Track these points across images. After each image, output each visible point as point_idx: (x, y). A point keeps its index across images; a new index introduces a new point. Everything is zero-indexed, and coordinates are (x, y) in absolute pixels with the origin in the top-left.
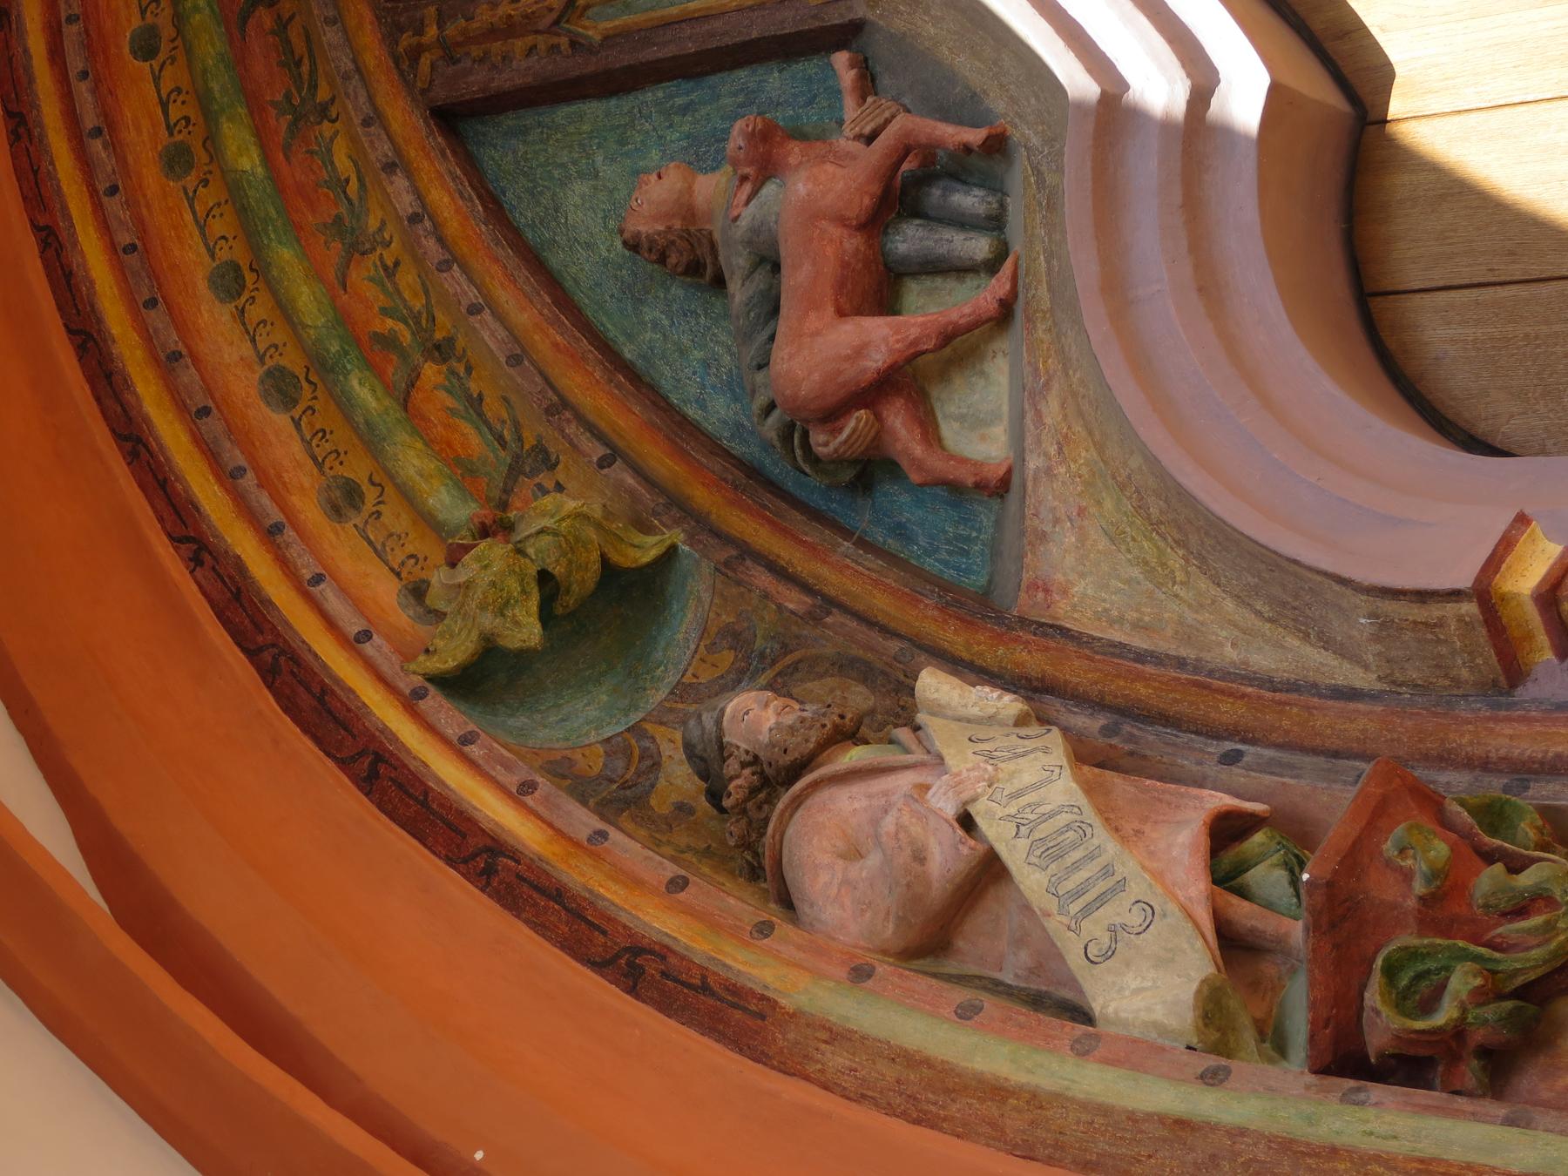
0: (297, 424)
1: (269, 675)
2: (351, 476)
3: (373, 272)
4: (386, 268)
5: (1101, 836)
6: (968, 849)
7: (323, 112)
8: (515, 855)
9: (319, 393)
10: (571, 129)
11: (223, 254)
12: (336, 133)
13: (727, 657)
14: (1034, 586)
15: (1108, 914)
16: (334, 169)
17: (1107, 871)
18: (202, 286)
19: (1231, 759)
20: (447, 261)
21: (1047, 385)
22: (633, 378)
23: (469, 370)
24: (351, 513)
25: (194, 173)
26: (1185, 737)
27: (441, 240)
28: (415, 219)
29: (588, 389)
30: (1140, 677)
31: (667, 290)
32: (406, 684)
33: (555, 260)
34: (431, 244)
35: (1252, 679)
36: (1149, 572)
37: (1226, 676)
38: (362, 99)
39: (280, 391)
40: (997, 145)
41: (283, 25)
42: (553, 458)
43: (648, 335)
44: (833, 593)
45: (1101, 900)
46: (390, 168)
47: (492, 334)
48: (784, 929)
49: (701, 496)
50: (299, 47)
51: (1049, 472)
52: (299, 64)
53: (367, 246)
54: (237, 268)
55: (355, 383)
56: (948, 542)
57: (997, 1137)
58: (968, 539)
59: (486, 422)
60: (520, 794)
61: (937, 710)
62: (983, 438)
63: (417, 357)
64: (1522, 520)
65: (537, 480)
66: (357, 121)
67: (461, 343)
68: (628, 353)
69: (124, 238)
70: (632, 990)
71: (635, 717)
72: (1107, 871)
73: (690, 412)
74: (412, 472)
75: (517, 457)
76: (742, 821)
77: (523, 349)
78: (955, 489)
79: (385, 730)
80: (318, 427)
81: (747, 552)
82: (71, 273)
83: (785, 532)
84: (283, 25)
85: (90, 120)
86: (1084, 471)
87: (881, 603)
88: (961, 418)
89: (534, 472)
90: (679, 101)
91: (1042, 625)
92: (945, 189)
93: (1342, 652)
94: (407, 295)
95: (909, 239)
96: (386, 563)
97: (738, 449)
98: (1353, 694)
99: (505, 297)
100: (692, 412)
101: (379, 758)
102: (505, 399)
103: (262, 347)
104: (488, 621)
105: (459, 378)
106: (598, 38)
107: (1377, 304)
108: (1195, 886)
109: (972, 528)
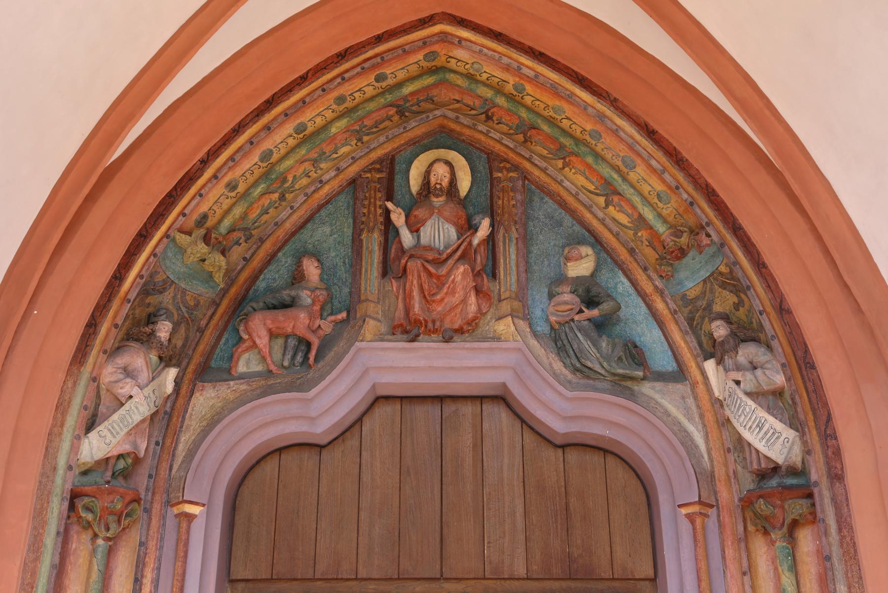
0: (255, 164)
1: (169, 195)
5: (126, 430)
6: (123, 400)
7: (360, 140)
8: (120, 286)
11: (309, 124)
13: (192, 303)
14: (203, 386)
15: (109, 435)
17: (118, 433)
18: (299, 121)
19: (157, 443)
22: (271, 258)
23: (276, 208)
26: (163, 431)
27: (314, 191)
28: (321, 182)
29: (268, 246)
30: (178, 418)
32: (172, 233)
33: (309, 225)
34: (313, 188)
35: (176, 445)
36: (203, 417)
37: (177, 439)
40: (310, 367)
41: (389, 118)
45: (112, 433)
46: (338, 169)
48: (105, 356)
49: (233, 290)
50: (381, 126)
52: (376, 127)
54: (305, 130)
57: (53, 426)
60: (140, 276)
61: (168, 373)
63: (280, 191)
64: (204, 505)
67: (284, 204)
68: (280, 254)
69: (307, 100)
70: (87, 325)
71: (177, 281)
72: (118, 433)
75: (249, 229)
76: (138, 332)
78: (231, 357)
79: (153, 236)
81: (218, 305)
83: (222, 316)
84: (389, 118)
85: (346, 76)
87: (201, 347)
89: (245, 235)
93: (178, 470)
98: (171, 470)
100: (262, 277)
101: (145, 237)
104: (189, 250)
107: (278, 453)
108: (115, 453)
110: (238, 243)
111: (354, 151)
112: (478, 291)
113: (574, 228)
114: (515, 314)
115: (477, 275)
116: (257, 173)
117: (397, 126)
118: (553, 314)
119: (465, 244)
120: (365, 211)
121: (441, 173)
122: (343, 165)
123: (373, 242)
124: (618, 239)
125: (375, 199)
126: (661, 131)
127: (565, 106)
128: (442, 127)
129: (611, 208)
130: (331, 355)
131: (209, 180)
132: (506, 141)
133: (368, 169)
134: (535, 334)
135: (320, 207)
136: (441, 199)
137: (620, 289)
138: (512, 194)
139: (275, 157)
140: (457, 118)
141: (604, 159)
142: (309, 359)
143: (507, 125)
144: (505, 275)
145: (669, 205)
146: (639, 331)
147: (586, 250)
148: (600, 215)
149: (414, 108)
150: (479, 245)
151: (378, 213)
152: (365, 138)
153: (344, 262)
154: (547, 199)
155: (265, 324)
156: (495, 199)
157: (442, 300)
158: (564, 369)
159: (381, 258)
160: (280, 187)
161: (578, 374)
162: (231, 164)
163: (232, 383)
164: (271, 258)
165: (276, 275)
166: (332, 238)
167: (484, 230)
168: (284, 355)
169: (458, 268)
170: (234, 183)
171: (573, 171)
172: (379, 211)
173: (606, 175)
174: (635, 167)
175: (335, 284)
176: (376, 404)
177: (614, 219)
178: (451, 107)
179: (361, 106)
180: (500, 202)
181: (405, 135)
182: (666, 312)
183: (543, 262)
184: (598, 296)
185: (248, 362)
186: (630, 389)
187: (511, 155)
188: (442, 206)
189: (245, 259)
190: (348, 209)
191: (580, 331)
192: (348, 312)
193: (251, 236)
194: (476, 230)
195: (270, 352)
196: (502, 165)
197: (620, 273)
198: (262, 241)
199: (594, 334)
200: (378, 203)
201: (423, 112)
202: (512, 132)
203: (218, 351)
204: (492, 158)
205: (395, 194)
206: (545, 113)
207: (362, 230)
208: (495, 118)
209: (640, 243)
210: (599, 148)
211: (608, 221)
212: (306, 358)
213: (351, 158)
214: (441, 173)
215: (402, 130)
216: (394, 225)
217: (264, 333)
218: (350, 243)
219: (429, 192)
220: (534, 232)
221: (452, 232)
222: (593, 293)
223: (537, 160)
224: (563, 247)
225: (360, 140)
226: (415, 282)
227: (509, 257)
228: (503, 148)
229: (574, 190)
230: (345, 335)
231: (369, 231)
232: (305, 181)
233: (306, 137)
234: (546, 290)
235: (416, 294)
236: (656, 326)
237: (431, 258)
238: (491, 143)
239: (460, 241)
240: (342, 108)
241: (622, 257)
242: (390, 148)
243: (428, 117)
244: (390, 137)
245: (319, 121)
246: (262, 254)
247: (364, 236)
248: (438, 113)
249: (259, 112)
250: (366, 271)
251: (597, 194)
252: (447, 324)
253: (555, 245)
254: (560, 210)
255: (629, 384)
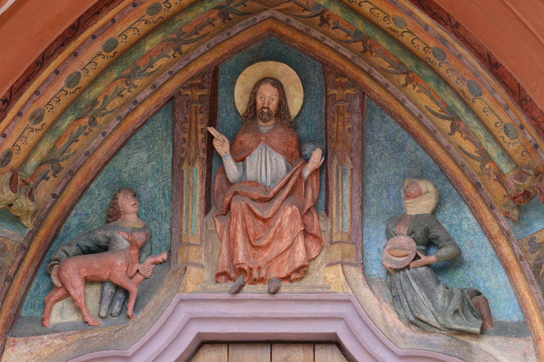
0: (62, 90)
2: (45, 117)
3: (119, 88)
4: (120, 92)
7: (178, 49)
9: (72, 94)
10: (165, 149)
11: (120, 40)
12: (169, 58)
14: (14, 341)
16: (156, 60)
18: (108, 38)
20: (121, 118)
21: (65, 339)
22: (84, 190)
24: (33, 122)
25: (150, 17)
27: (128, 114)
28: (135, 102)
29: (78, 179)
31: (110, 198)
33: (124, 151)
34: (127, 110)
38: (179, 67)
39: (72, 79)
42: (57, 175)
43: (97, 193)
44: (14, 282)
47: (96, 143)
49: (42, 232)
50: (202, 32)
51: (43, 342)
52: (196, 33)
53: (129, 82)
54: (115, 47)
55: (71, 118)
56: (34, 302)
58: (35, 308)
59: (69, 145)
62: (57, 315)
65: (50, 170)
66: (170, 70)
67: (95, 129)
68: (93, 186)
69: (117, 18)
73: (73, 212)
74: (42, 149)
77: (91, 155)
80: (61, 98)
82: (99, 13)
84: (211, 23)
86: (42, 353)
88: (63, 308)
89: (53, 167)
90: (166, 192)
91: (4, 346)
92: (122, 298)
94: (112, 102)
95: (109, 290)
96: (17, 140)
97: (62, 230)
99: (107, 145)
100: (73, 212)
102: (76, 151)
103: (87, 67)
105: (83, 131)
106: (183, 168)
109: (37, 309)
110: (45, 177)
111: (171, 64)
112: (306, 233)
113: (418, 153)
114: (347, 260)
115: (305, 213)
116: (65, 100)
117: (220, 32)
118: (388, 259)
119: (294, 179)
120: (186, 136)
121: (268, 95)
122: (160, 81)
123: (195, 176)
124: (463, 172)
125: (196, 122)
126: (504, 64)
127: (407, 19)
128: (271, 31)
129: (457, 134)
130: (150, 305)
131: (14, 119)
132: (343, 51)
133: (190, 85)
134: (369, 281)
135: (135, 131)
136: (270, 123)
137: (465, 226)
138: (347, 115)
139: (84, 81)
140: (288, 20)
141: (447, 84)
142: (127, 309)
143: (345, 30)
144: (337, 215)
145: (516, 140)
146: (484, 275)
147: (426, 186)
148: (445, 142)
149: (238, 8)
150: (311, 175)
151: (200, 139)
152: (184, 48)
153: (164, 194)
154: (388, 117)
155: (79, 273)
156: (329, 120)
157: (269, 245)
158: (398, 321)
159: (204, 192)
160: (90, 110)
161: (412, 327)
162: (35, 97)
163: (45, 337)
164: (84, 190)
165: (90, 210)
166: (149, 166)
167: (316, 158)
168: (101, 303)
169: (285, 210)
170: (39, 114)
171: (417, 88)
172: (201, 136)
173: (450, 104)
174: (481, 94)
175: (154, 219)
176: (202, 351)
177: (460, 148)
178: (281, 7)
179: (178, 18)
180: (335, 125)
181: (228, 42)
182: (511, 258)
183: (381, 193)
184: (437, 239)
185: (61, 313)
186: (467, 344)
187: (349, 67)
188: (270, 132)
189: (54, 196)
190: (167, 130)
191: (415, 280)
192: (169, 252)
193: (60, 169)
194: (307, 161)
195: (85, 303)
196: (337, 80)
197: (466, 209)
198: (72, 174)
199: (431, 283)
200: (200, 127)
201: (249, 14)
202: (349, 38)
203: (28, 297)
204: (327, 69)
205: (219, 112)
206: (385, 25)
207: (183, 159)
208: (331, 22)
209: (487, 177)
210: (442, 70)
211: (453, 150)
212: (124, 307)
213: (167, 70)
214: (268, 95)
215: (225, 37)
216: (217, 153)
217: (78, 282)
218: (169, 171)
219: (255, 114)
220: (373, 158)
221: (281, 162)
222: (432, 234)
223: (376, 74)
224: (404, 176)
225: (178, 49)
226: (239, 227)
227: (344, 191)
228: (339, 59)
229: (416, 111)
230: (166, 280)
231: (190, 164)
232: (117, 102)
233: (119, 57)
234: (384, 227)
235: (240, 239)
236: (502, 270)
237: (256, 197)
238: (326, 52)
239: (288, 176)
240: (156, 18)
241: (467, 193)
242: (212, 59)
243: (255, 19)
244: (212, 45)
245: (132, 36)
246: (72, 188)
247: (185, 167)
248: (266, 14)
249: (64, 41)
250: (188, 209)
251: (443, 117)
252: (274, 274)
253: (395, 174)
254: (403, 132)
255: (466, 339)
